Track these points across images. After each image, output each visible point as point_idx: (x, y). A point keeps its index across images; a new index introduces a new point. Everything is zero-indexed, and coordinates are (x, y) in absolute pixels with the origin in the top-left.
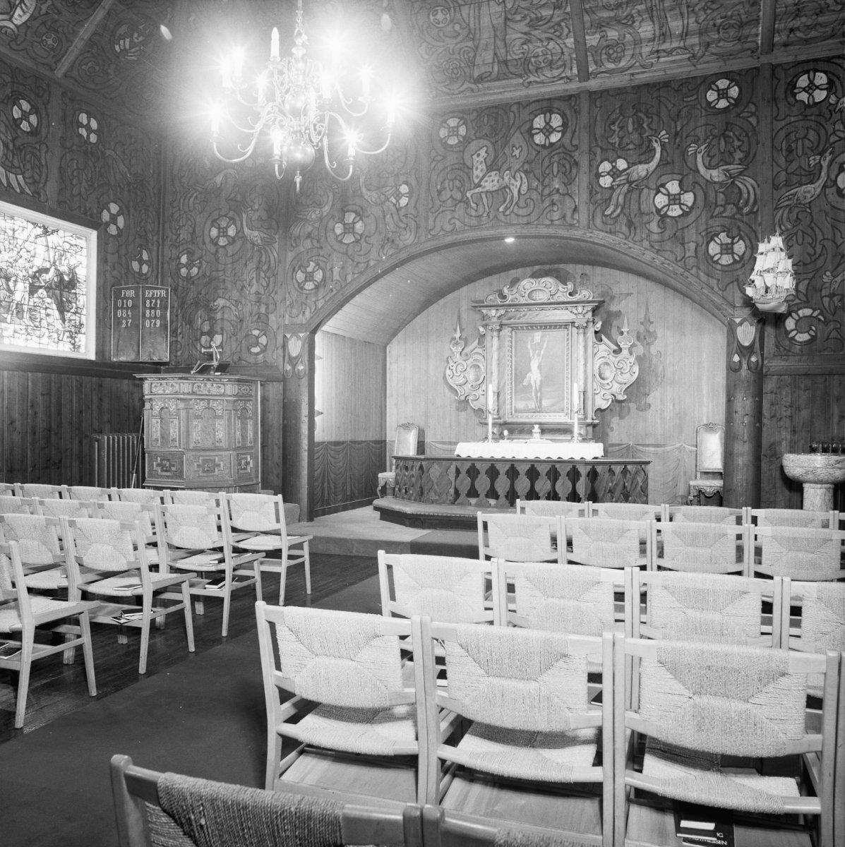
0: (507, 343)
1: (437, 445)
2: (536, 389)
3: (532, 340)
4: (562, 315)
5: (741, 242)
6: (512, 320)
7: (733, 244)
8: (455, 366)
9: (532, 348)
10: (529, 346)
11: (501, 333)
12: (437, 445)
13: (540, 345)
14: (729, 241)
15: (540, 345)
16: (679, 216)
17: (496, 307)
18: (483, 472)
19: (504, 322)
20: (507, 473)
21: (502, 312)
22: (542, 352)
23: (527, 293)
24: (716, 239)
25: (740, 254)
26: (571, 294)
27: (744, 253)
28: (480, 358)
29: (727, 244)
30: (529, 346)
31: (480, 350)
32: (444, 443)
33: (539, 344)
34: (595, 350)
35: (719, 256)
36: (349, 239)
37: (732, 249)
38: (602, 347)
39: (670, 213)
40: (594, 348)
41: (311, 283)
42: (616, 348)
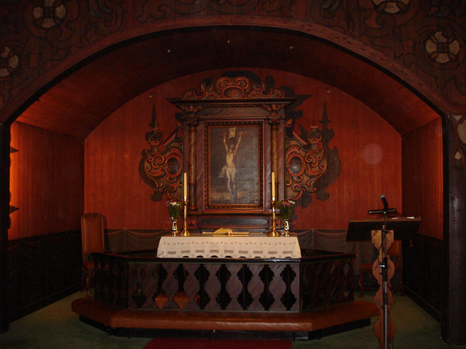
0: (203, 138)
1: (133, 233)
2: (231, 183)
3: (228, 135)
4: (255, 113)
5: (456, 42)
6: (209, 116)
7: (448, 43)
8: (153, 160)
9: (227, 143)
10: (224, 141)
11: (197, 128)
12: (133, 233)
13: (234, 140)
14: (444, 40)
15: (234, 140)
16: (396, 14)
17: (194, 103)
18: (278, 301)
19: (202, 117)
20: (239, 274)
21: (200, 107)
22: (237, 147)
23: (223, 91)
24: (432, 37)
25: (456, 54)
26: (264, 93)
27: (459, 53)
28: (177, 151)
29: (443, 43)
30: (224, 141)
31: (177, 145)
32: (135, 231)
33: (232, 138)
34: (287, 146)
35: (436, 54)
36: (48, 24)
37: (448, 48)
38: (293, 143)
39: (387, 10)
40: (285, 143)
41: (5, 70)
42: (305, 144)
